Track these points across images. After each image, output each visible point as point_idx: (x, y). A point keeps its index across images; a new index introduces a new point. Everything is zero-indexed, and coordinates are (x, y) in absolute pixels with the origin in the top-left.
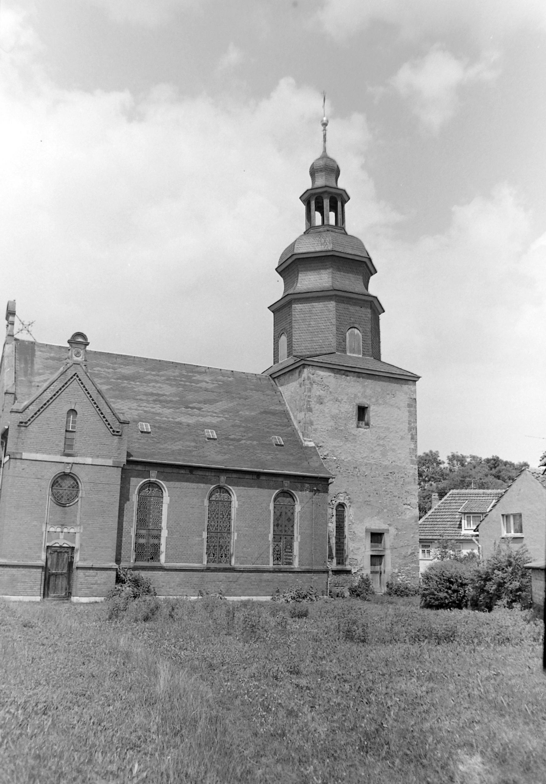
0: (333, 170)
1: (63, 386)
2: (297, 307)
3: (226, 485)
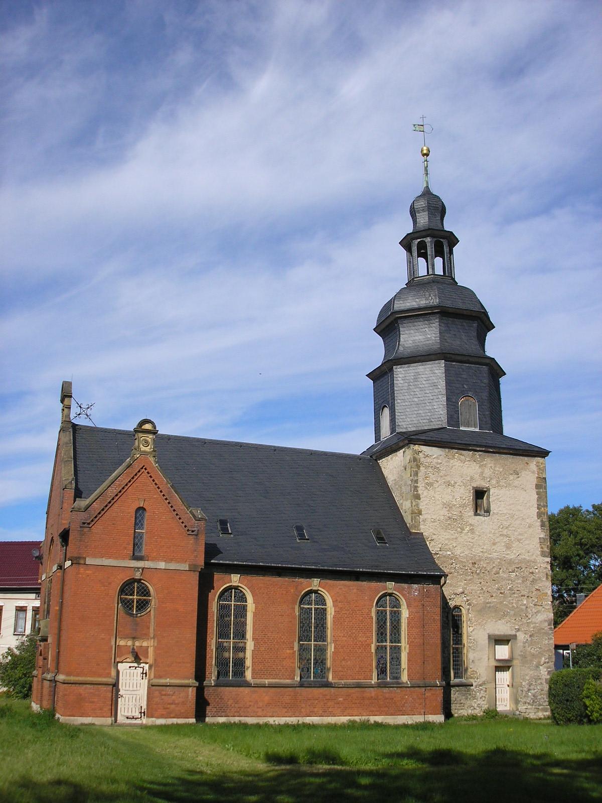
0: (437, 208)
1: (130, 482)
2: (400, 372)
3: (320, 589)
